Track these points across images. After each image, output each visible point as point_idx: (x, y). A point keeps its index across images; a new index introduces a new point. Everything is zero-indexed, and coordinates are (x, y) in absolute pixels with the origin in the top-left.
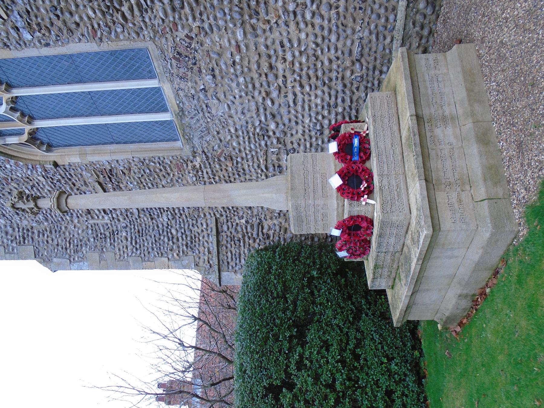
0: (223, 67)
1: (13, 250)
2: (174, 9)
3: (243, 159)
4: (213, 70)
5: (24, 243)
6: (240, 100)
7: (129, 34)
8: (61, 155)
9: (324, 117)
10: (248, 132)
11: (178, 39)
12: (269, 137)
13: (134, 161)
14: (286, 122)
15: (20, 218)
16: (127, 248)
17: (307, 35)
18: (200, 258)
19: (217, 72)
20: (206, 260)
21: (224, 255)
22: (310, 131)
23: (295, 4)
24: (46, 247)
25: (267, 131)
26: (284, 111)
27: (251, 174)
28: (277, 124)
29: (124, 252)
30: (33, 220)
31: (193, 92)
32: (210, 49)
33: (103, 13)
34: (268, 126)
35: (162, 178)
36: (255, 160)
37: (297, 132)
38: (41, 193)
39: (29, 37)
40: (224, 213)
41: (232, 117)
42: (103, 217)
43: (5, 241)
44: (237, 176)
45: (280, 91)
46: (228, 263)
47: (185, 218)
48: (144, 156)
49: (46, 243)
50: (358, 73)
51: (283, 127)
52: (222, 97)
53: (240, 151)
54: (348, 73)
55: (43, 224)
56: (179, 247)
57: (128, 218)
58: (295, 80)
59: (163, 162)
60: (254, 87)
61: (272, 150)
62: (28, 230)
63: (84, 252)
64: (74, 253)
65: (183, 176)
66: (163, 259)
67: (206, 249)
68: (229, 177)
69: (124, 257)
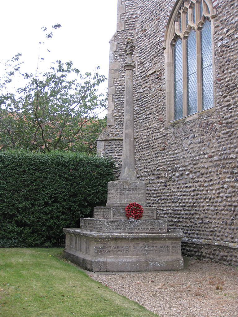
0: (203, 148)
1: (122, 18)
2: (227, 123)
3: (163, 156)
4: (203, 142)
5: (126, 25)
6: (189, 157)
7: (218, 98)
8: (169, 52)
9: (180, 203)
10: (175, 160)
11: (215, 125)
12: (172, 172)
13: (165, 93)
14: (179, 182)
15: (140, 23)
16: (120, 85)
17: (214, 194)
18: (113, 129)
19: (201, 144)
20: (112, 133)
21: (114, 143)
22: (174, 195)
23: (227, 188)
24: (123, 37)
25: (175, 171)
26: (183, 181)
27: (156, 161)
28: (178, 177)
29: (118, 83)
30: (139, 30)
31: (194, 131)
32: (211, 141)
33: (227, 86)
34: (178, 172)
35: (156, 109)
36: (163, 164)
37: (174, 188)
38: (152, 37)
39: (219, 46)
40: (138, 144)
41: (182, 151)
42: (139, 71)
43: (128, 14)
44: (155, 153)
45: (192, 179)
46: (109, 146)
47: (136, 120)
48: (166, 99)
49: (126, 37)
50: (198, 222)
51: (176, 180)
52: (191, 147)
53: (167, 155)
54: (198, 216)
55: (137, 36)
56: (120, 116)
57: (138, 86)
58: (196, 187)
59: (163, 110)
60: (195, 164)
61: (166, 174)
62: (133, 27)
63: (119, 60)
64: (119, 54)
65: (157, 121)
66: (114, 107)
67: (118, 133)
68: (155, 148)
69: (116, 84)
